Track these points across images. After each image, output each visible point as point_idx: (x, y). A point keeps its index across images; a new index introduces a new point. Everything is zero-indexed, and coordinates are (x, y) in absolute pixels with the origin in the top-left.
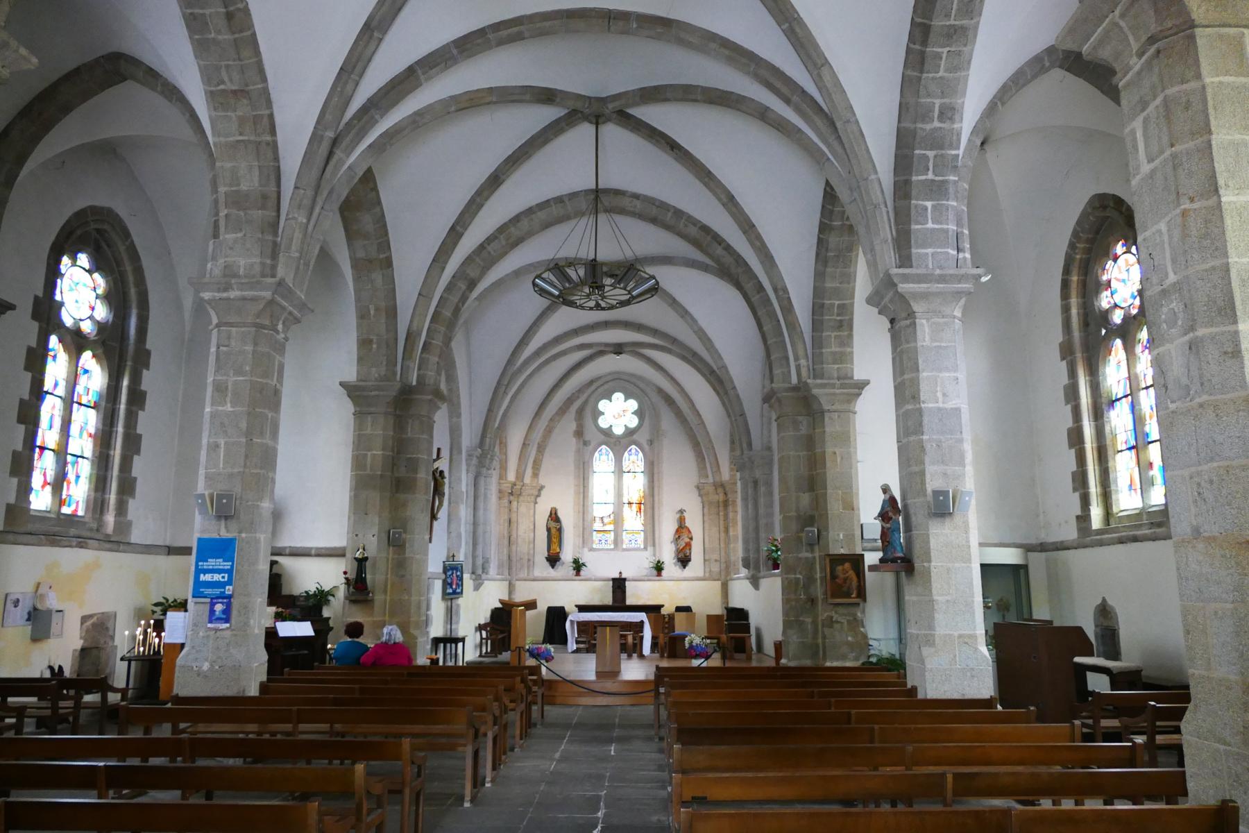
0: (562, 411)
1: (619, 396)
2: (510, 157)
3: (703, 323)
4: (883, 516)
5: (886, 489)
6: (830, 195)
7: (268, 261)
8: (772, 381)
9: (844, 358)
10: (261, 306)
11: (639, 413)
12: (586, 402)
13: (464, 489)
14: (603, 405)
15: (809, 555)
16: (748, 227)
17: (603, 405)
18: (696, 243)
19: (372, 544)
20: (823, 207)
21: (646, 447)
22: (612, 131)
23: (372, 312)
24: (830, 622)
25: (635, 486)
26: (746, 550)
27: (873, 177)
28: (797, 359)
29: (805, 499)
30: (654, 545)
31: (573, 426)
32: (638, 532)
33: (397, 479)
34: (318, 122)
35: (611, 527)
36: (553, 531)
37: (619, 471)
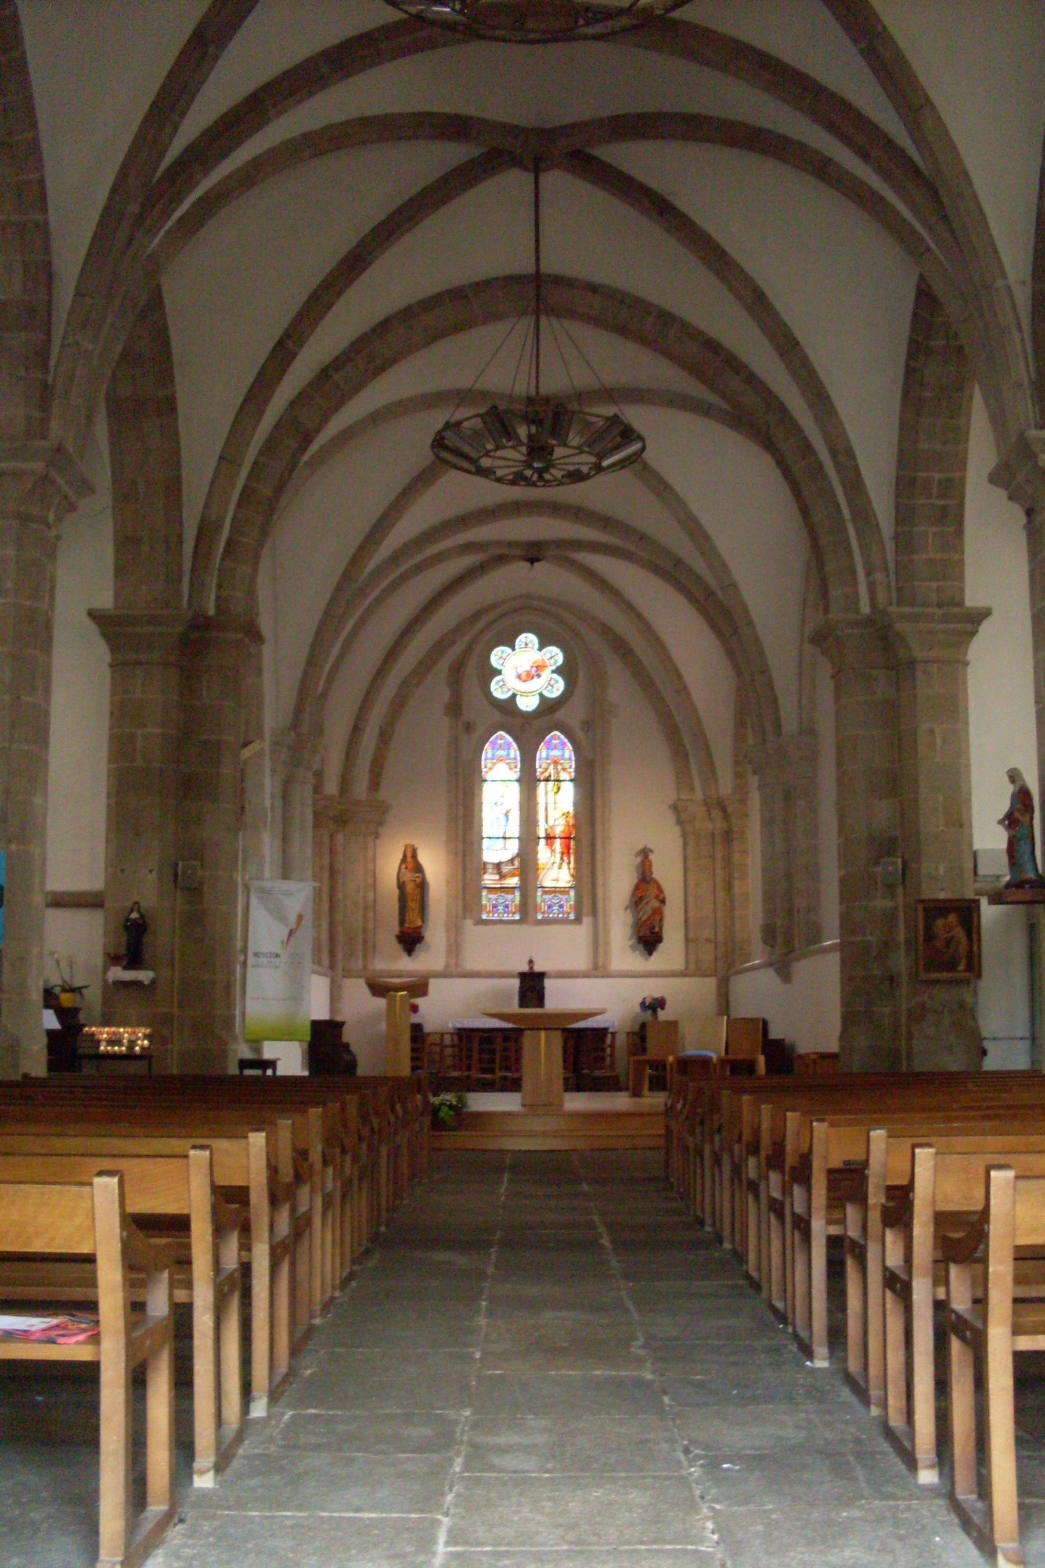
0: (425, 666)
1: (528, 639)
2: (382, 224)
4: (1011, 821)
5: (1014, 776)
6: (925, 298)
7: (37, 414)
8: (826, 611)
9: (951, 570)
10: (30, 486)
11: (565, 671)
13: (268, 804)
14: (498, 656)
15: (888, 904)
16: (787, 346)
17: (498, 656)
18: (695, 369)
19: (148, 891)
20: (915, 315)
21: (580, 735)
22: (558, 182)
23: (141, 488)
24: (918, 1014)
25: (558, 804)
26: (770, 913)
27: (1000, 283)
28: (869, 573)
29: (883, 811)
30: (594, 913)
31: (444, 694)
32: (564, 891)
33: (176, 785)
34: (114, 190)
35: (513, 881)
37: (529, 781)
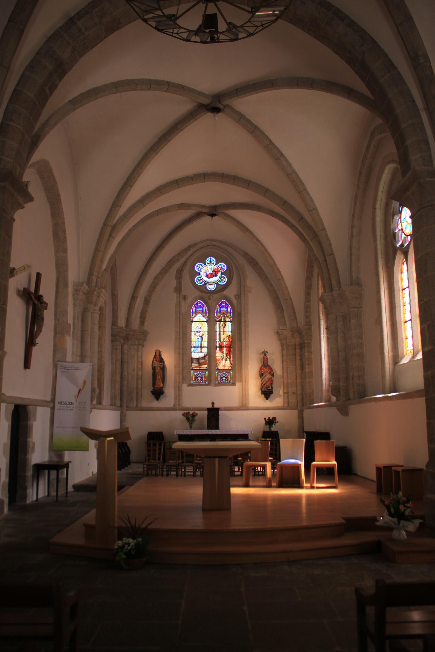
3: (298, 166)
11: (229, 273)
12: (184, 264)
31: (174, 283)
36: (158, 369)
